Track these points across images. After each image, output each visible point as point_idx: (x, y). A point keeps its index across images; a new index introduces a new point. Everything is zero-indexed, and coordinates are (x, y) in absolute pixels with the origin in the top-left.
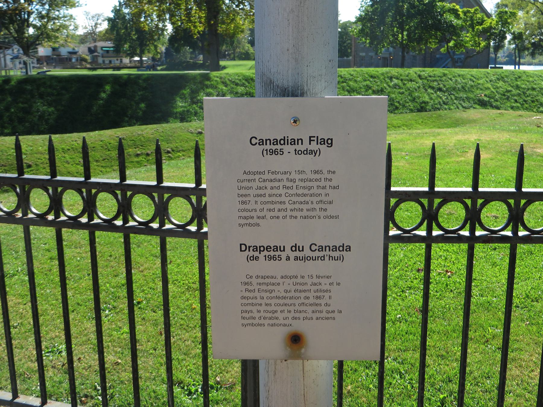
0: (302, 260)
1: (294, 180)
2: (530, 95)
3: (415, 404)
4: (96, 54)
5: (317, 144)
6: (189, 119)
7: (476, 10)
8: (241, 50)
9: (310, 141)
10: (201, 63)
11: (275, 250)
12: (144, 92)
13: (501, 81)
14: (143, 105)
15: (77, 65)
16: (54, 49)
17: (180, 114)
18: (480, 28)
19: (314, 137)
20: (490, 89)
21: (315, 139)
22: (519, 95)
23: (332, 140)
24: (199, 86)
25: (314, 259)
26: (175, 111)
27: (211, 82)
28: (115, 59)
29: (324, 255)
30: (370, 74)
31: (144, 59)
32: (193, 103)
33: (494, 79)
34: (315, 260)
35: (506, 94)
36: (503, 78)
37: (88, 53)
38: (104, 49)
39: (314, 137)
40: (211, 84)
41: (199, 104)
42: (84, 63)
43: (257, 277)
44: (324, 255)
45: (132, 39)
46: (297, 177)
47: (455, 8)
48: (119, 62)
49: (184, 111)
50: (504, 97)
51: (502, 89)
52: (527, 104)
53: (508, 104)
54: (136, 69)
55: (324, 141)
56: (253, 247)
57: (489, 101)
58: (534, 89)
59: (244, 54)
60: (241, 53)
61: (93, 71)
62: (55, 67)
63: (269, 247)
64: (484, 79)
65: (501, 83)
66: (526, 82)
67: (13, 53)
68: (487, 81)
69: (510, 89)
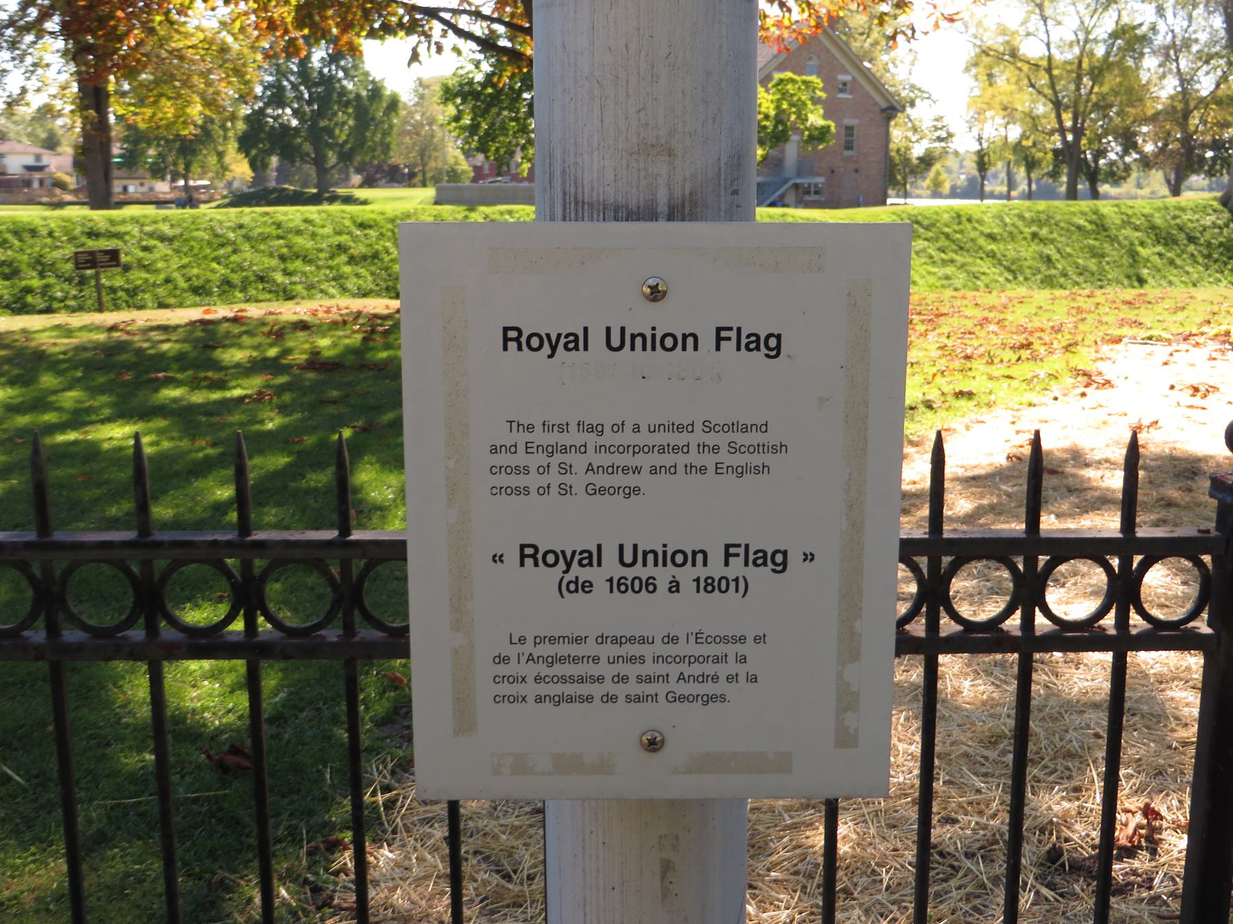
1: (600, 428)
9: (719, 339)
15: (41, 196)
21: (733, 334)
28: (137, 182)
30: (359, 221)
42: (58, 191)
43: (600, 640)
54: (153, 206)
61: (53, 210)
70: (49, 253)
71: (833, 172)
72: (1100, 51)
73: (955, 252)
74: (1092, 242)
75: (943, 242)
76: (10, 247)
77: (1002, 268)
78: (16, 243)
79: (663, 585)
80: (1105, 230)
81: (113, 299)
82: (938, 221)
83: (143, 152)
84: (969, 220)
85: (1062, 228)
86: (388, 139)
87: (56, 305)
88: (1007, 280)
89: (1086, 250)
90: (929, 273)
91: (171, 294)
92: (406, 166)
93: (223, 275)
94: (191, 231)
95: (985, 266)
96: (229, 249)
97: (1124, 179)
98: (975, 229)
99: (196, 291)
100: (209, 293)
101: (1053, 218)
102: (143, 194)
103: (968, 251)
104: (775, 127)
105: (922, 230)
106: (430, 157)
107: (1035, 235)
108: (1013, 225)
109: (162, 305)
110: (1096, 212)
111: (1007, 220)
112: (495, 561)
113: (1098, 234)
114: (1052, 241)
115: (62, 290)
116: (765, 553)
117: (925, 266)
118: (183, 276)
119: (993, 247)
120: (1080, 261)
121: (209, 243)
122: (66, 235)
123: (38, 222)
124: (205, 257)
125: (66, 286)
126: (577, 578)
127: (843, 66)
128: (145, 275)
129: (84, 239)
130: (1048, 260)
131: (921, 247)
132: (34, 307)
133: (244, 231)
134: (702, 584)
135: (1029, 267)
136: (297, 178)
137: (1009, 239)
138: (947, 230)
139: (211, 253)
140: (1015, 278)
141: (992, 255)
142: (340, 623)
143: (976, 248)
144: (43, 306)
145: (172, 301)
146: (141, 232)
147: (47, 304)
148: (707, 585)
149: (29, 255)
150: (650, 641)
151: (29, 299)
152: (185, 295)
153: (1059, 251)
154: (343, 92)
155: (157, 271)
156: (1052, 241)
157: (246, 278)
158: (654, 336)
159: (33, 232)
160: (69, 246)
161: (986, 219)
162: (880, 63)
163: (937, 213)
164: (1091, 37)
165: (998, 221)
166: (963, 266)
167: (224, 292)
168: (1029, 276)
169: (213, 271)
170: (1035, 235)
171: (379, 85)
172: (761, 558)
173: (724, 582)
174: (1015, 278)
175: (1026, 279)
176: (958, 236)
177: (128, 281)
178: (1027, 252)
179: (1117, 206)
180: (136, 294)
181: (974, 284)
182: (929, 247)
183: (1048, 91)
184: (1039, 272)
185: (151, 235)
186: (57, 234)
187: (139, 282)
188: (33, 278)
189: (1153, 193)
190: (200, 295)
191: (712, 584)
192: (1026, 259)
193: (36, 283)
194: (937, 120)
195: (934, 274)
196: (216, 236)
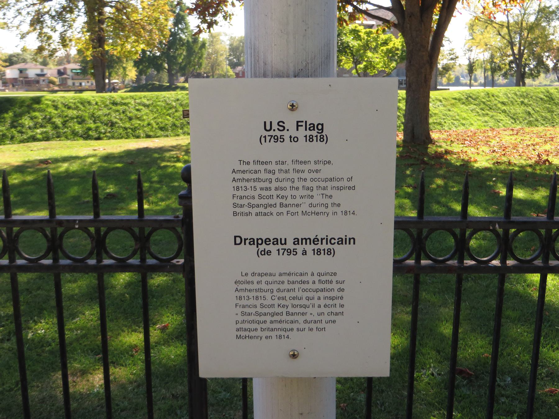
4: (65, 76)
5: (306, 130)
9: (298, 126)
11: (275, 243)
15: (44, 88)
16: (21, 71)
18: (384, 48)
19: (303, 122)
21: (304, 124)
23: (322, 125)
28: (86, 81)
32: (13, 126)
37: (57, 76)
39: (303, 122)
41: (19, 128)
42: (51, 85)
46: (276, 168)
47: (357, 29)
54: (74, 92)
55: (314, 127)
56: (250, 239)
62: (17, 90)
63: (268, 240)
70: (97, 112)
72: (532, 19)
73: (488, 110)
74: (547, 105)
75: (482, 106)
76: (80, 110)
77: (509, 117)
78: (83, 108)
79: (300, 252)
80: (553, 100)
81: (126, 133)
82: (479, 96)
84: (493, 96)
85: (534, 99)
86: (201, 61)
87: (102, 136)
88: (512, 123)
89: (545, 109)
90: (478, 120)
91: (151, 131)
92: (205, 73)
93: (172, 122)
94: (157, 102)
95: (502, 116)
96: (174, 110)
97: (537, 77)
98: (496, 100)
99: (162, 129)
100: (167, 130)
101: (529, 95)
102: (89, 86)
104: (402, 53)
105: (472, 100)
106: (216, 69)
107: (522, 102)
108: (512, 98)
109: (148, 136)
110: (548, 92)
111: (509, 96)
113: (550, 102)
114: (530, 105)
115: (104, 129)
117: (476, 117)
118: (155, 122)
119: (504, 108)
120: (543, 114)
121: (165, 107)
122: (103, 104)
123: (90, 98)
124: (164, 114)
125: (105, 127)
126: (265, 249)
128: (139, 122)
129: (111, 106)
130: (529, 113)
131: (473, 108)
132: (93, 136)
133: (179, 102)
135: (521, 117)
136: (156, 79)
137: (511, 104)
138: (483, 100)
139: (166, 112)
140: (515, 122)
141: (504, 111)
143: (497, 108)
144: (97, 136)
145: (151, 133)
146: (135, 102)
147: (98, 135)
149: (89, 113)
150: (274, 275)
151: (90, 133)
152: (157, 131)
153: (533, 109)
154: (181, 39)
155: (144, 120)
156: (530, 105)
157: (182, 123)
159: (89, 103)
160: (105, 109)
161: (500, 95)
162: (96, 35)
163: (478, 92)
164: (527, 12)
165: (505, 96)
166: (492, 117)
167: (173, 129)
168: (521, 121)
169: (168, 120)
170: (522, 102)
172: (341, 241)
174: (515, 122)
175: (520, 122)
176: (489, 103)
177: (132, 125)
178: (520, 110)
179: (557, 89)
180: (136, 131)
181: (498, 124)
182: (476, 108)
183: (507, 37)
184: (526, 119)
185: (139, 104)
186: (99, 104)
187: (137, 125)
188: (91, 123)
189: (540, 83)
190: (163, 131)
192: (519, 113)
193: (93, 126)
194: (451, 50)
196: (168, 104)
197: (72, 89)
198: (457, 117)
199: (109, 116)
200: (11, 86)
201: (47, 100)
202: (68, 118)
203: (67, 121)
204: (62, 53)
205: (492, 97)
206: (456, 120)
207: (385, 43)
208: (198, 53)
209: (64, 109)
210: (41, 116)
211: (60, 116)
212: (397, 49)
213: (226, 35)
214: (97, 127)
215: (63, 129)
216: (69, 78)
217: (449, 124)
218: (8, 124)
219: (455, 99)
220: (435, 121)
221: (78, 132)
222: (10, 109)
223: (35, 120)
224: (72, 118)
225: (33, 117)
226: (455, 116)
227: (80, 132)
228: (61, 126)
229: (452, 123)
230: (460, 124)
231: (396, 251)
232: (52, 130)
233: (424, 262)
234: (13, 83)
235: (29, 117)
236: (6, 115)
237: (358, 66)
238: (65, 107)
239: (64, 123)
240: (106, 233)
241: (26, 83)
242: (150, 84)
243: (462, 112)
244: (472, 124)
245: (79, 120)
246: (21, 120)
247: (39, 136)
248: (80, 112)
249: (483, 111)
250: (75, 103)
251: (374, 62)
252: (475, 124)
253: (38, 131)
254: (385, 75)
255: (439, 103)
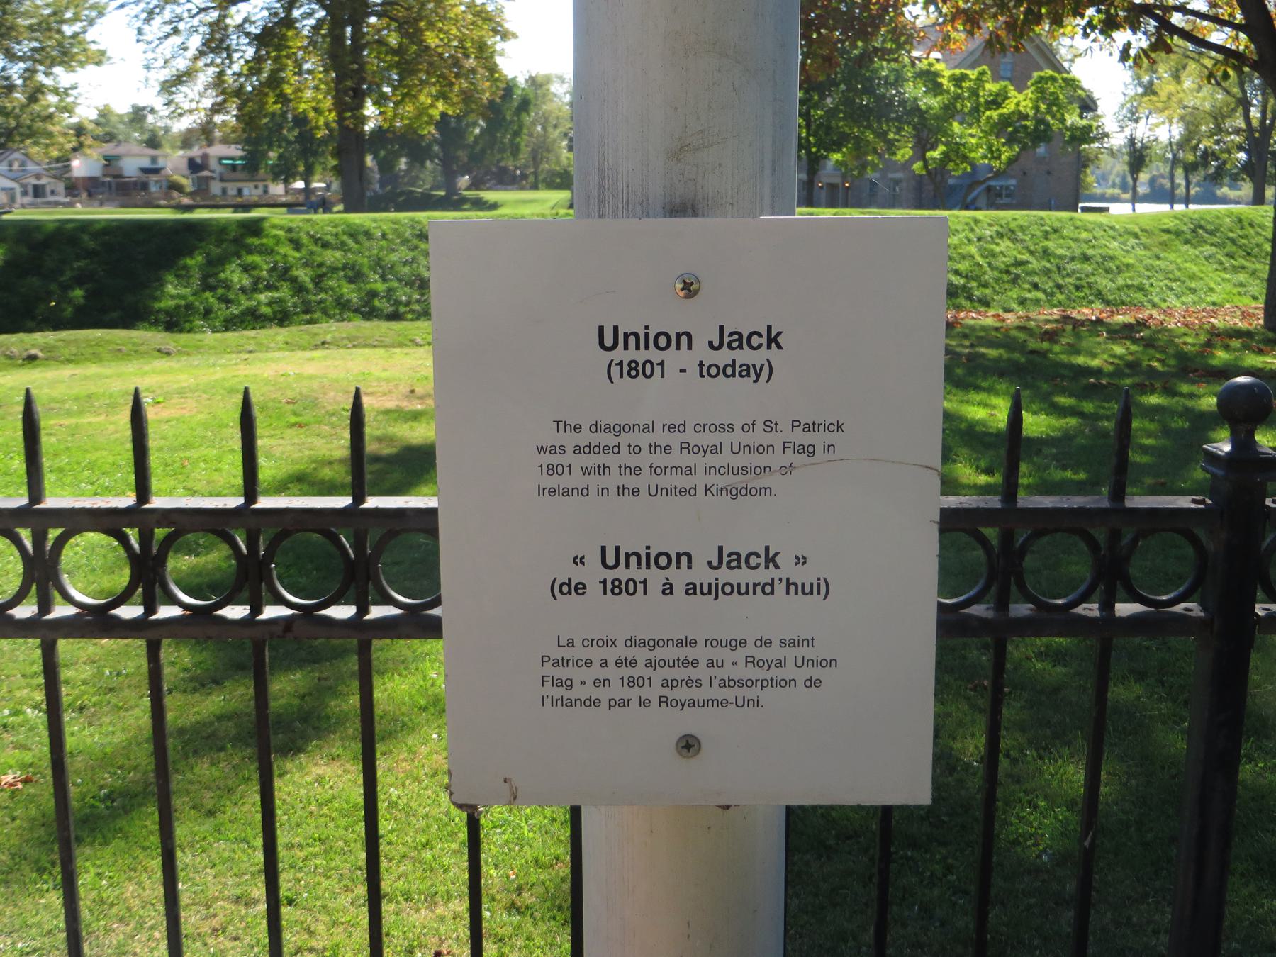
0: (710, 593)
2: (1074, 272)
3: (467, 952)
4: (205, 173)
6: (187, 325)
7: (982, 73)
8: (553, 167)
10: (442, 197)
12: (88, 261)
13: (1005, 239)
14: (78, 293)
15: (159, 199)
17: (168, 313)
18: (994, 114)
20: (973, 257)
22: (1047, 272)
24: (232, 248)
25: (743, 590)
26: (157, 305)
27: (261, 238)
28: (251, 185)
29: (773, 580)
31: (316, 185)
32: (207, 286)
33: (988, 233)
34: (747, 593)
35: (1013, 270)
36: (1013, 231)
37: (187, 172)
38: (225, 162)
40: (262, 245)
41: (220, 291)
42: (175, 194)
44: (773, 580)
45: (286, 139)
47: (933, 69)
48: (260, 191)
49: (178, 307)
50: (1006, 277)
51: (1004, 259)
52: (1062, 293)
53: (1014, 294)
54: (231, 210)
57: (964, 287)
58: (1086, 258)
59: (559, 175)
60: (553, 174)
61: (184, 213)
62: (102, 204)
64: (962, 235)
65: (1004, 245)
66: (1070, 242)
67: (11, 170)
68: (969, 240)
69: (1025, 257)
71: (1025, 173)
73: (1244, 258)
75: (1230, 248)
83: (264, 155)
84: (1251, 225)
87: (402, 309)
90: (1223, 280)
102: (260, 196)
103: (1256, 257)
112: (576, 563)
115: (405, 294)
116: (739, 555)
125: (407, 290)
127: (1038, 63)
129: (415, 241)
131: (1210, 252)
132: (382, 310)
134: (609, 586)
138: (1231, 235)
142: (35, 600)
148: (614, 587)
149: (369, 257)
151: (377, 303)
158: (647, 335)
159: (368, 234)
163: (1218, 217)
171: (511, 84)
173: (631, 585)
176: (1244, 241)
191: (619, 587)
193: (380, 287)
195: (1229, 281)
197: (202, 203)
198: (1178, 274)
199: (415, 265)
200: (84, 195)
201: (275, 227)
202: (324, 270)
203: (324, 275)
204: (194, 122)
205: (1250, 229)
206: (1175, 280)
207: (996, 102)
208: (512, 122)
209: (314, 248)
210: (267, 263)
211: (306, 265)
212: (1026, 117)
213: (563, 82)
214: (390, 290)
215: (315, 295)
216: (213, 178)
217: (1162, 289)
218: (196, 282)
219: (1168, 231)
220: (1130, 282)
221: (349, 301)
222: (196, 248)
223: (255, 273)
224: (334, 269)
225: (248, 265)
226: (1171, 272)
227: (355, 300)
228: (311, 286)
229: (1166, 286)
230: (1185, 290)
231: (945, 586)
232: (292, 296)
233: (1124, 609)
234: (91, 188)
235: (239, 265)
236: (189, 262)
237: (928, 154)
238: (316, 244)
239: (318, 280)
240: (168, 542)
241: (117, 189)
242: (402, 193)
243: (1186, 261)
244: (1211, 290)
245: (350, 273)
246: (223, 271)
247: (265, 310)
248: (350, 255)
249: (1232, 261)
250: (336, 235)
251: (963, 145)
252: (1218, 288)
253: (263, 297)
254: (990, 175)
255: (1132, 241)
